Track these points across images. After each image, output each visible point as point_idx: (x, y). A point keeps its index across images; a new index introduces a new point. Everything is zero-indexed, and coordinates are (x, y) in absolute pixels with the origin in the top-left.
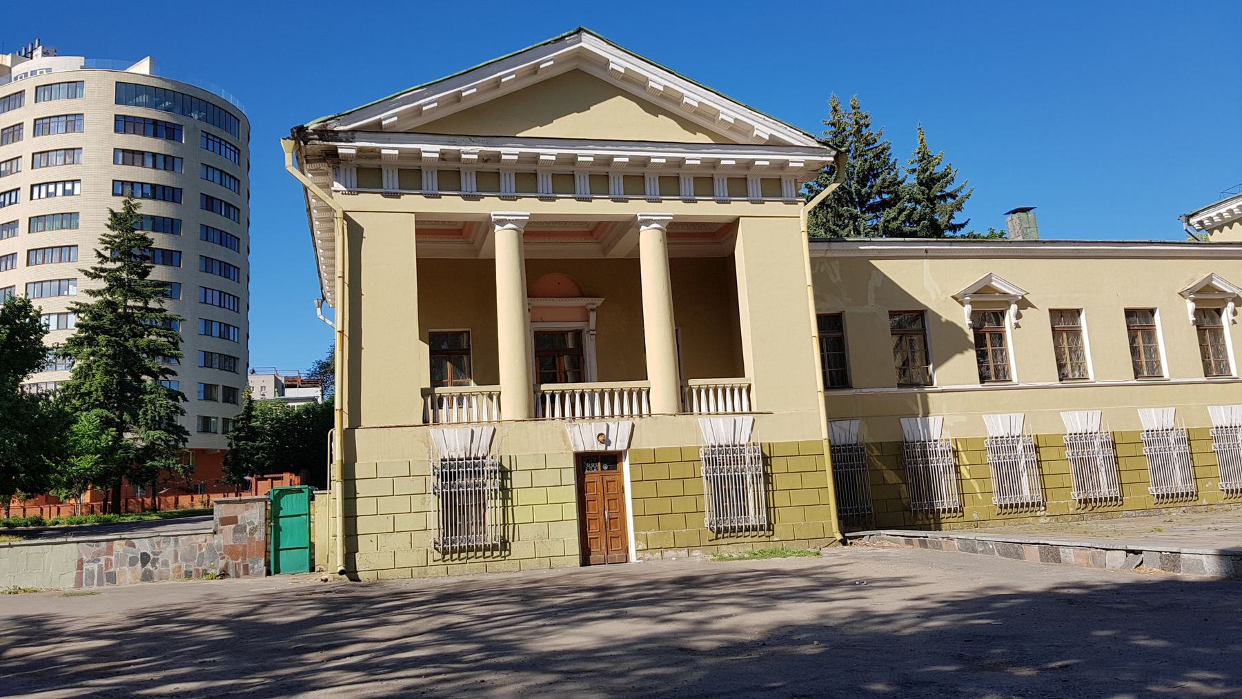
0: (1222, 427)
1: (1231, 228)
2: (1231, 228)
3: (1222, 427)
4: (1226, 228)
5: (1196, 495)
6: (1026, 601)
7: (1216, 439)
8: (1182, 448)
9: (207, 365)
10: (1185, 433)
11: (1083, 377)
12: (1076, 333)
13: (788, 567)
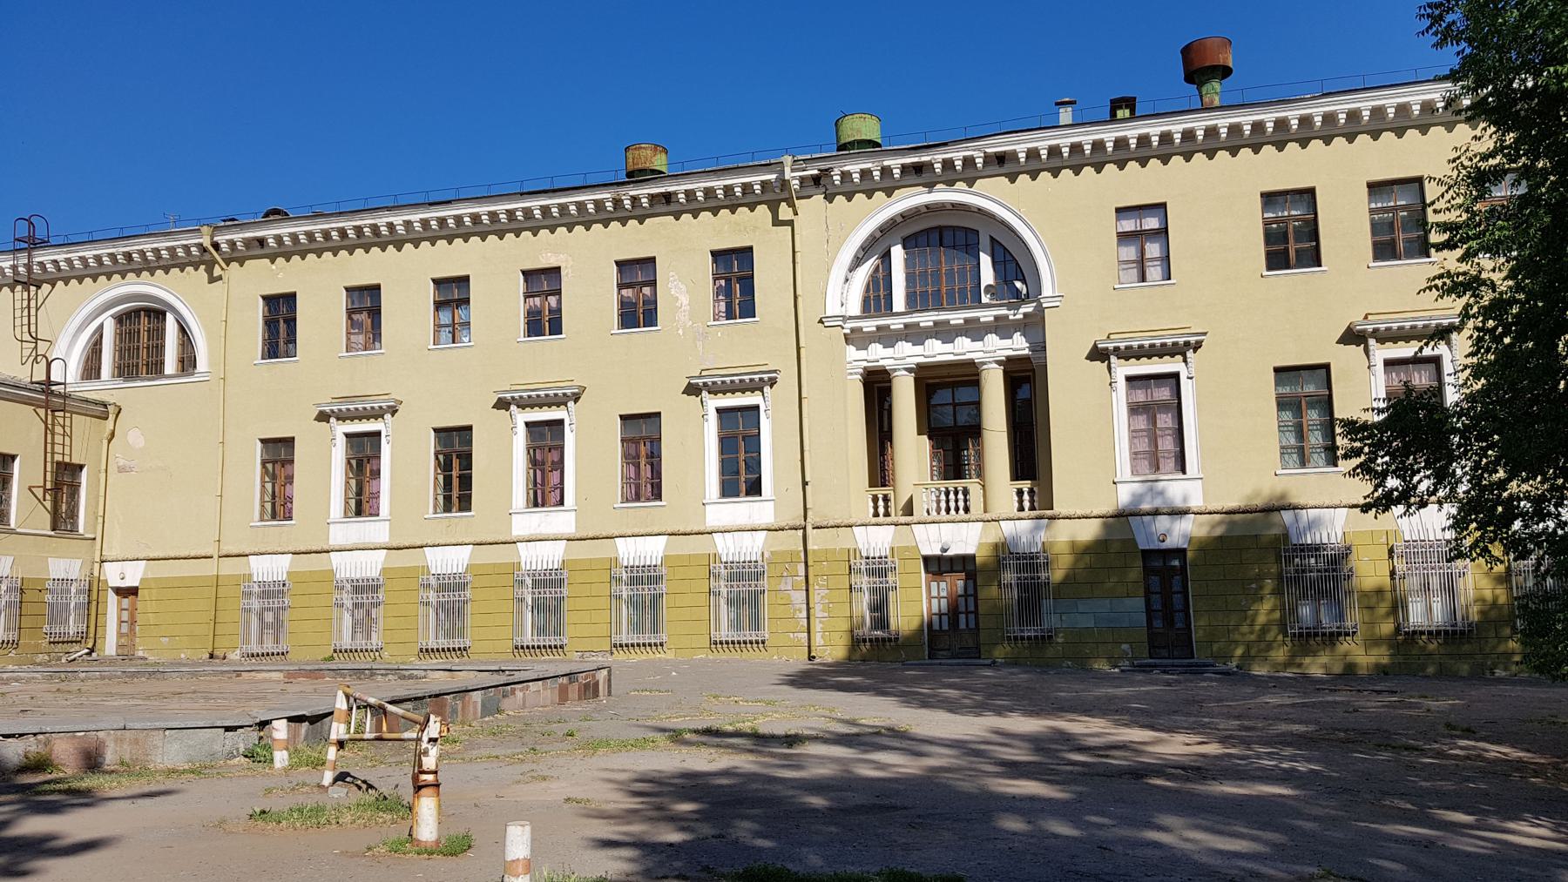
0: (67, 580)
1: (66, 285)
2: (66, 285)
3: (67, 580)
4: (74, 282)
5: (17, 644)
6: (1179, 785)
7: (51, 592)
8: (13, 597)
9: (955, 568)
10: (87, 585)
11: (74, 529)
12: (74, 489)
13: (850, 700)
